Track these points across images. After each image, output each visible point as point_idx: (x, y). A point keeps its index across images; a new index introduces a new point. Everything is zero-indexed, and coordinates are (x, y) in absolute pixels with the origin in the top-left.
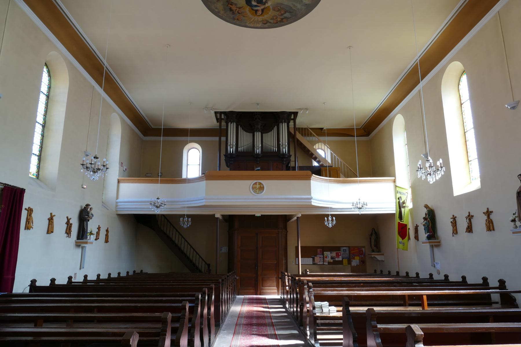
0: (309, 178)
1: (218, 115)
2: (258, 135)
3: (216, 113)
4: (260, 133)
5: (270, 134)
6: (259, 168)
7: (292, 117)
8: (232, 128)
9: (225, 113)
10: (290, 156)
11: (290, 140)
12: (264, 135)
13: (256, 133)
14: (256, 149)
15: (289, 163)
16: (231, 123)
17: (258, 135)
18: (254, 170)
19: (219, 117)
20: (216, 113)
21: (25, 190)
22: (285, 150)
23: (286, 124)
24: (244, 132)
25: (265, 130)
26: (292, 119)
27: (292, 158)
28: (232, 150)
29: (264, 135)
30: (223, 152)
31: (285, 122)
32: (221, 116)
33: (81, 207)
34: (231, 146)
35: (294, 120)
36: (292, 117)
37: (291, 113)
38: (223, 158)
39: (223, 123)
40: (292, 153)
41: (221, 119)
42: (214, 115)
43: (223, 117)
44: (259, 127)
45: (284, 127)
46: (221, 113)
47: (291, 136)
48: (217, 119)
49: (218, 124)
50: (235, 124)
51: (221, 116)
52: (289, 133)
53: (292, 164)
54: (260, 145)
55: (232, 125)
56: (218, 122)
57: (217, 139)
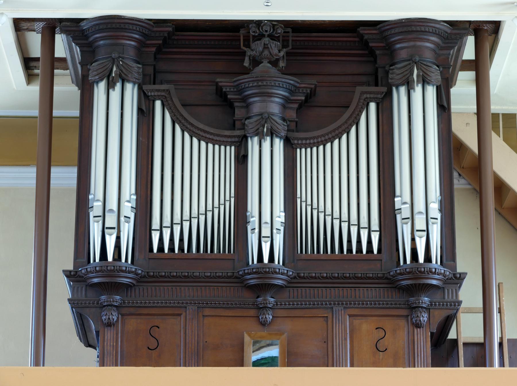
0: (356, 87)
1: (35, 42)
2: (267, 156)
3: (19, 25)
4: (279, 145)
5: (338, 147)
6: (274, 352)
7: (469, 52)
8: (116, 108)
9: (72, 27)
10: (457, 279)
11: (459, 184)
12: (302, 154)
13: (253, 144)
14: (253, 239)
15: (448, 322)
16: (110, 86)
17: (267, 156)
18: (240, 362)
19: (36, 50)
20: (19, 25)
21: (27, 85)
22: (421, 229)
23: (431, 92)
24: (185, 141)
25: (311, 123)
26: (467, 65)
27: (470, 294)
28: (113, 231)
29: (302, 154)
30: (62, 256)
31: (425, 81)
32: (49, 44)
33: (114, 90)
34: (111, 221)
35: (479, 67)
36: (469, 52)
37: (458, 29)
38: (60, 290)
39: (66, 88)
40: (468, 261)
41: (54, 63)
42: (9, 35)
43: (61, 46)
44: (275, 108)
45: (416, 109)
46: (51, 27)
47: (460, 162)
48: (28, 63)
49: (35, 89)
50: (131, 91)
51: (49, 44)
52: (451, 149)
53: (468, 328)
54: (280, 217)
55: (115, 94)
56: (30, 77)
57: (27, 176)
